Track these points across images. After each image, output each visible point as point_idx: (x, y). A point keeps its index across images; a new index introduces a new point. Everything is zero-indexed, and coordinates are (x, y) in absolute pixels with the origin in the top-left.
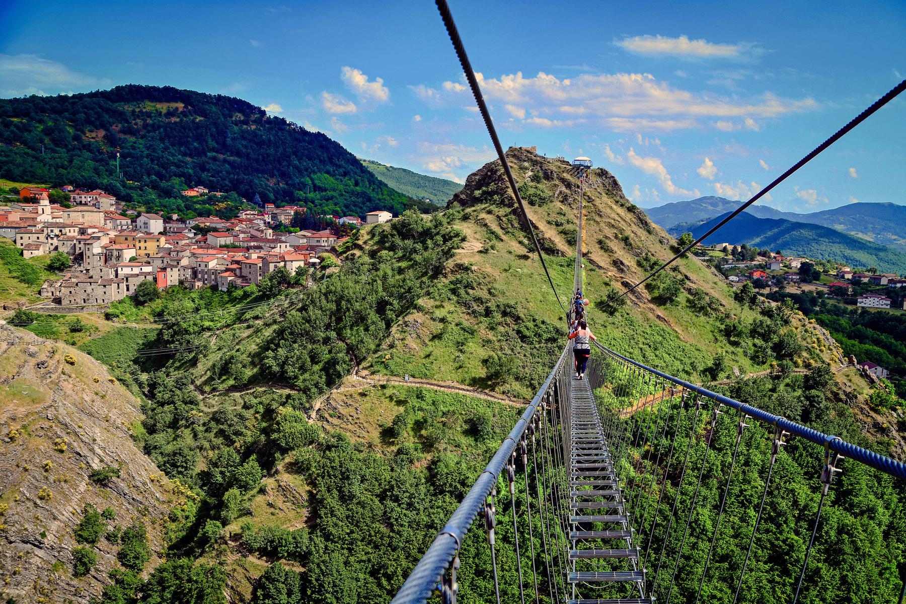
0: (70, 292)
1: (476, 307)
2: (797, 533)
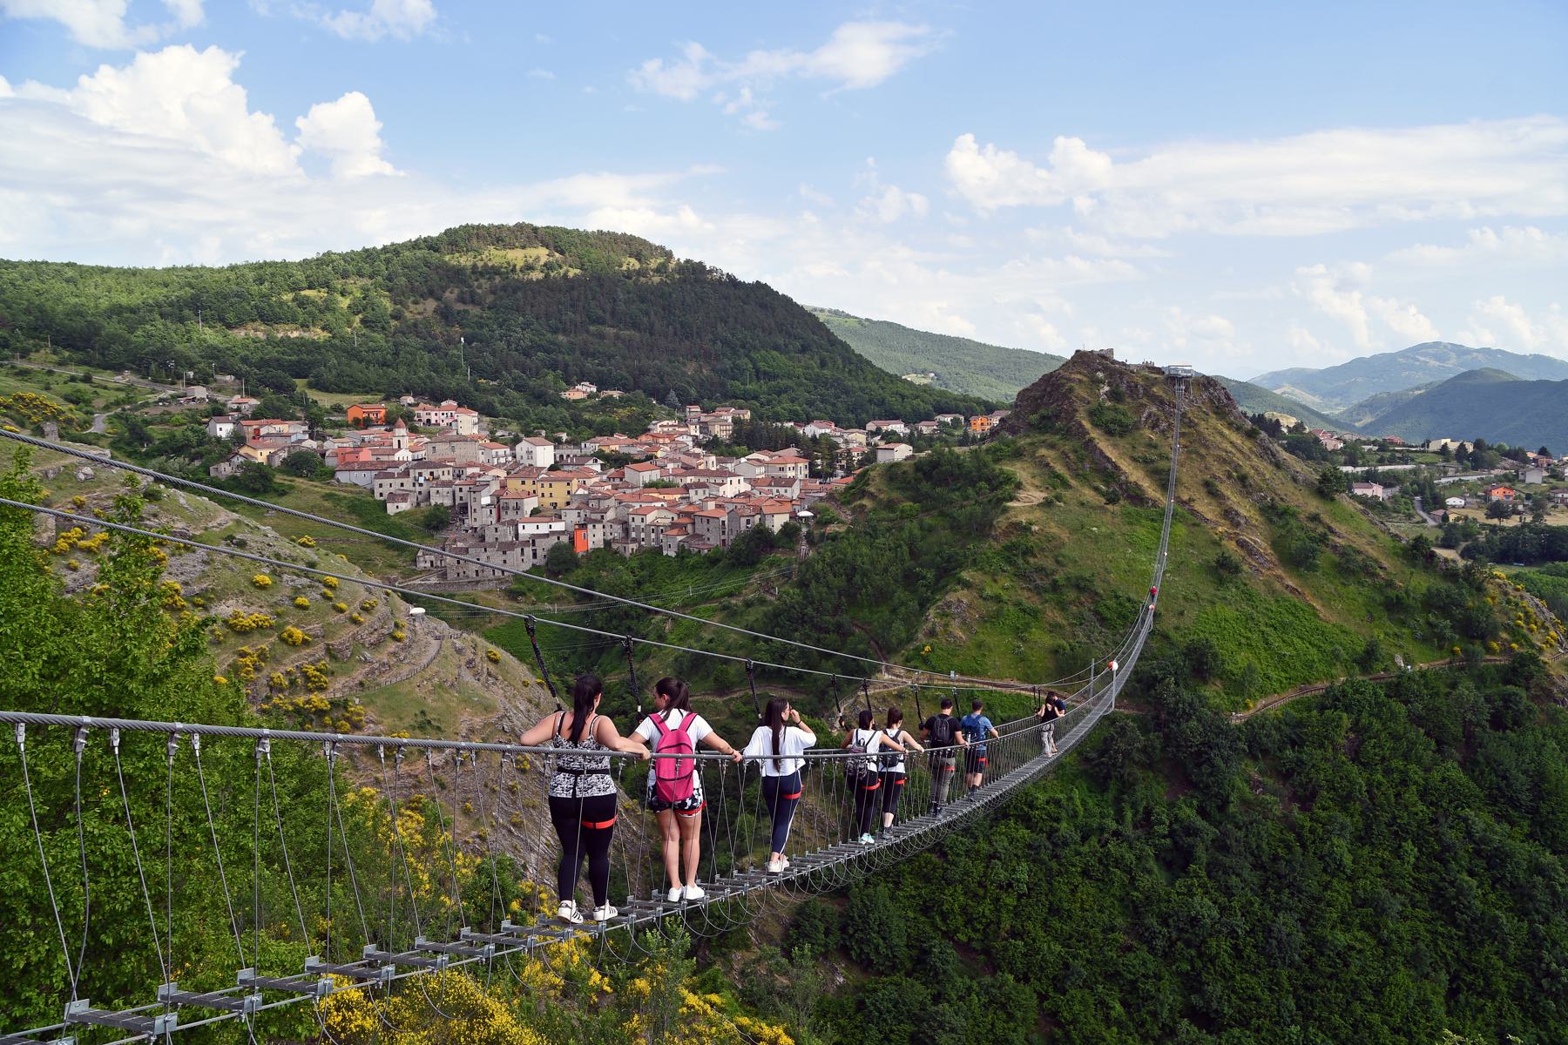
1: (1038, 582)
2: (1471, 874)
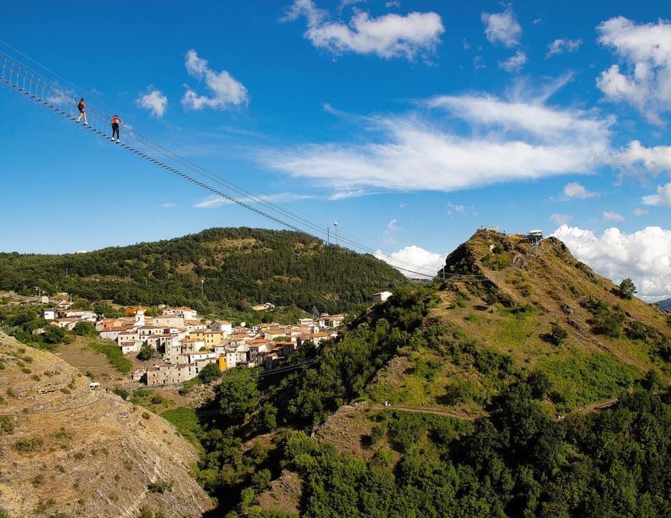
0: (154, 375)
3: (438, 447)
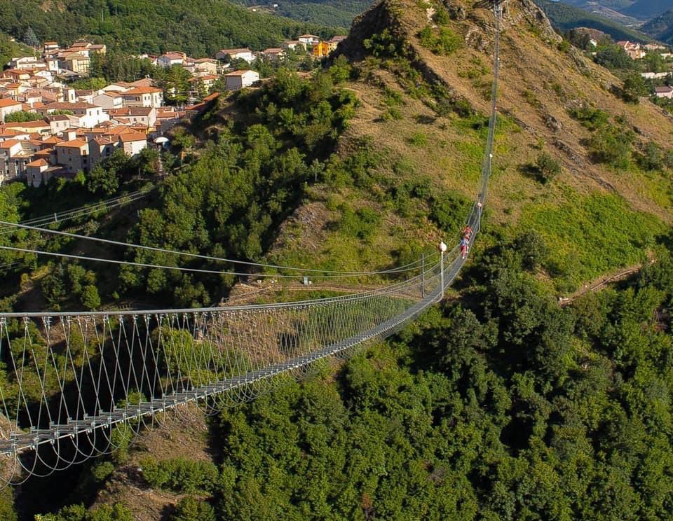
3: (393, 347)
